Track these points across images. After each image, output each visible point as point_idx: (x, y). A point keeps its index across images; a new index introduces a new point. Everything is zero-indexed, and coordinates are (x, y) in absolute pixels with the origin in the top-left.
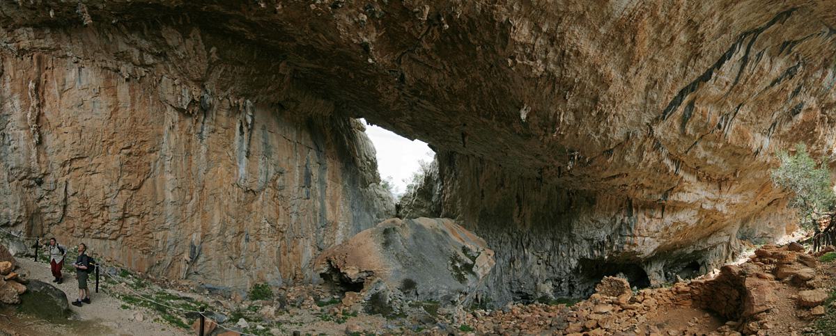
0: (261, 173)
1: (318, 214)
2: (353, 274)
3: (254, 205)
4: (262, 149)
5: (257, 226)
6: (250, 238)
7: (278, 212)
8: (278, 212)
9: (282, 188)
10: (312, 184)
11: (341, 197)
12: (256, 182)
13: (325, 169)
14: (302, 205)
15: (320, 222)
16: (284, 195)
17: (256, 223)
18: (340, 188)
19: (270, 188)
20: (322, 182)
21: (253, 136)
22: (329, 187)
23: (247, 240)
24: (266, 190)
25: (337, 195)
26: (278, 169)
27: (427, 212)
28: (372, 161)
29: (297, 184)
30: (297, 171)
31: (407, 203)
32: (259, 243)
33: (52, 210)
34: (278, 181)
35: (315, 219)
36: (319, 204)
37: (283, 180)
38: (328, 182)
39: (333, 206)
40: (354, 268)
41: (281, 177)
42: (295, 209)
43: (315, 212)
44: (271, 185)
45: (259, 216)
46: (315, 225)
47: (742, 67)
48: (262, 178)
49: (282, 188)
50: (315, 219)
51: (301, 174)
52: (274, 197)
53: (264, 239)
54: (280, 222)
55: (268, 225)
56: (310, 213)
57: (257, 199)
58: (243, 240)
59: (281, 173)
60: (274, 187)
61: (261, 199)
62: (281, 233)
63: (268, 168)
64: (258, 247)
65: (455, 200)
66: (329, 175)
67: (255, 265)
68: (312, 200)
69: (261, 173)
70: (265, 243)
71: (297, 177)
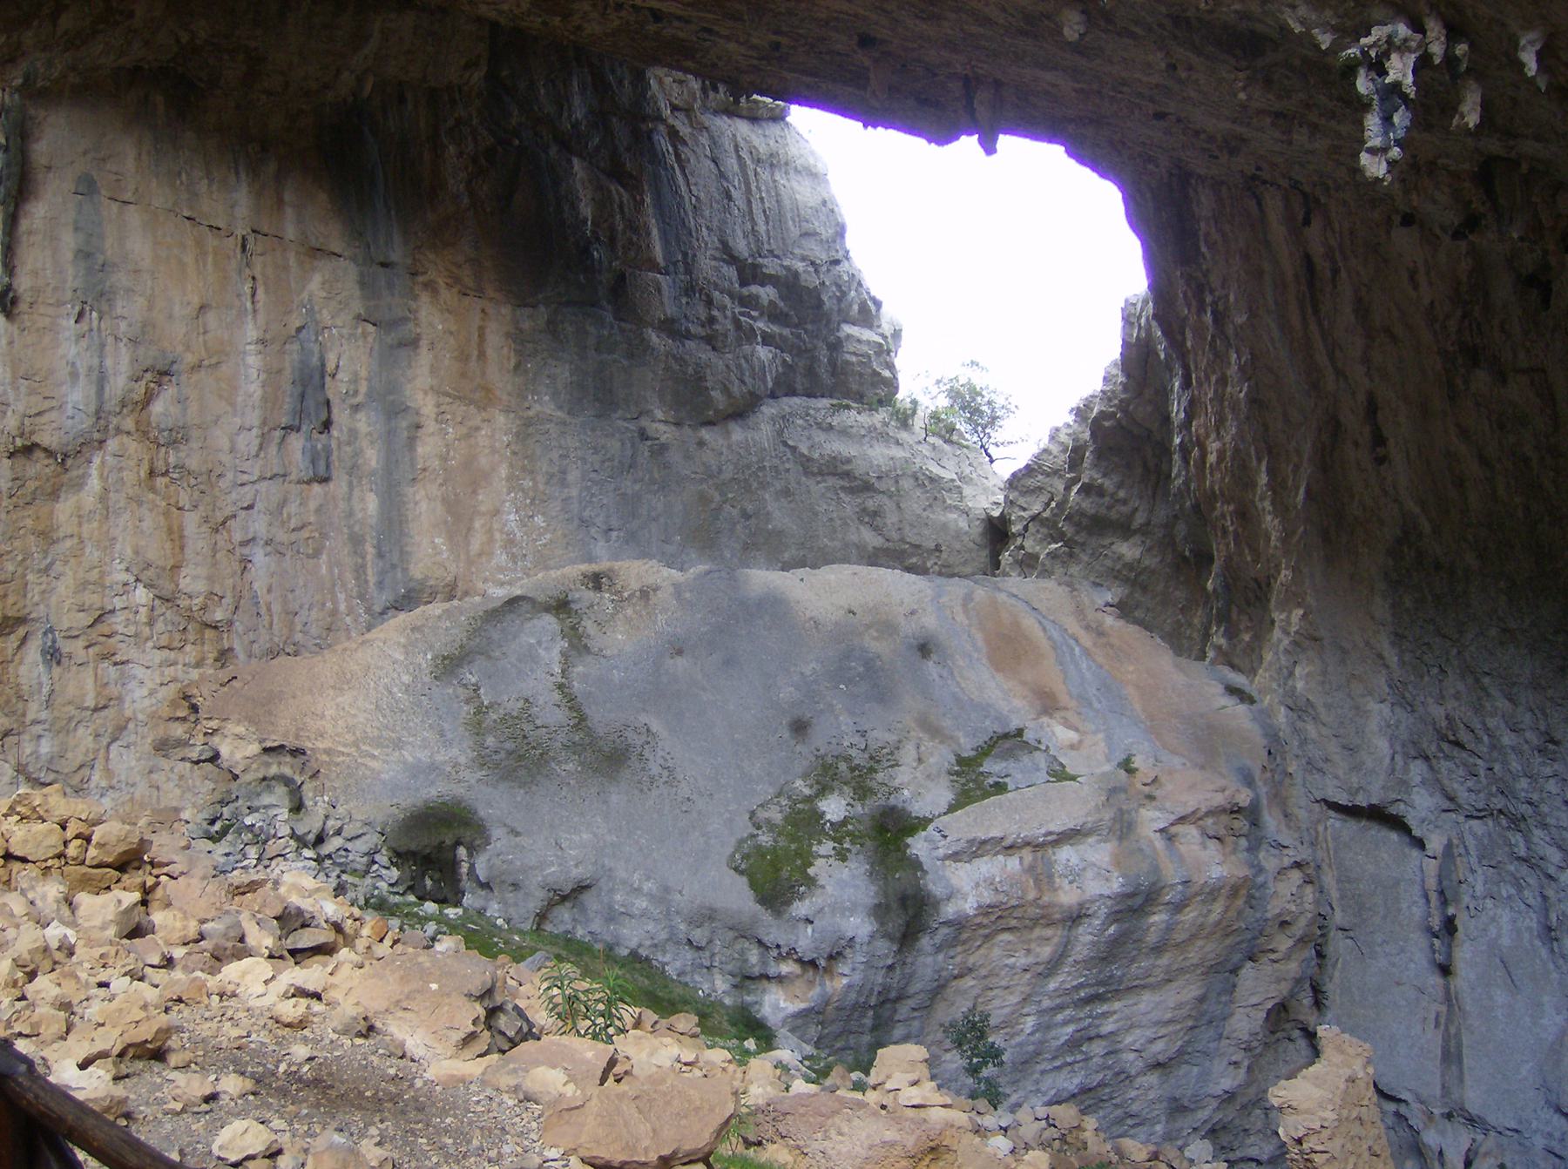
0: (74, 375)
1: (370, 550)
2: (238, 756)
3: (64, 510)
4: (72, 277)
5: (92, 599)
6: (66, 647)
7: (177, 537)
8: (177, 537)
9: (177, 437)
10: (340, 415)
11: (503, 471)
12: (53, 415)
13: (413, 343)
14: (293, 508)
15: (380, 585)
16: (193, 463)
17: (83, 586)
18: (497, 429)
19: (125, 439)
20: (393, 408)
21: (24, 224)
22: (431, 426)
23: (53, 656)
24: (112, 444)
25: (484, 461)
26: (148, 355)
27: (1151, 562)
28: (790, 285)
29: (254, 418)
30: (253, 361)
31: (1036, 508)
32: (113, 672)
33: (231, 857)
34: (157, 408)
35: (360, 570)
36: (372, 504)
37: (181, 401)
38: (427, 406)
39: (458, 518)
40: (240, 730)
41: (169, 391)
42: (259, 525)
43: (356, 541)
44: (129, 424)
45: (92, 554)
46: (361, 596)
47: (44, 411)
48: (78, 396)
49: (177, 437)
50: (360, 570)
51: (272, 374)
52: (152, 473)
53: (133, 653)
54: (193, 582)
55: (141, 595)
56: (337, 544)
57: (79, 484)
58: (33, 652)
59: (166, 373)
60: (143, 432)
61: (94, 483)
62: (209, 633)
63: (102, 356)
64: (114, 690)
65: (1242, 477)
66: (434, 370)
67: (108, 772)
68: (339, 485)
69: (74, 375)
70: (139, 672)
71: (252, 387)
